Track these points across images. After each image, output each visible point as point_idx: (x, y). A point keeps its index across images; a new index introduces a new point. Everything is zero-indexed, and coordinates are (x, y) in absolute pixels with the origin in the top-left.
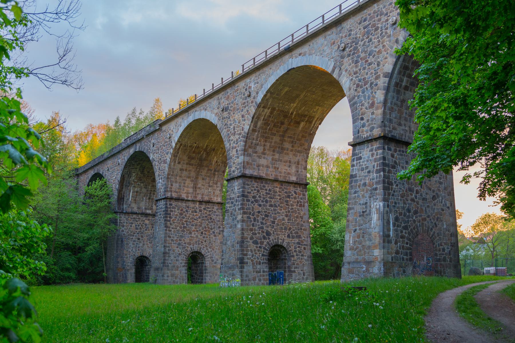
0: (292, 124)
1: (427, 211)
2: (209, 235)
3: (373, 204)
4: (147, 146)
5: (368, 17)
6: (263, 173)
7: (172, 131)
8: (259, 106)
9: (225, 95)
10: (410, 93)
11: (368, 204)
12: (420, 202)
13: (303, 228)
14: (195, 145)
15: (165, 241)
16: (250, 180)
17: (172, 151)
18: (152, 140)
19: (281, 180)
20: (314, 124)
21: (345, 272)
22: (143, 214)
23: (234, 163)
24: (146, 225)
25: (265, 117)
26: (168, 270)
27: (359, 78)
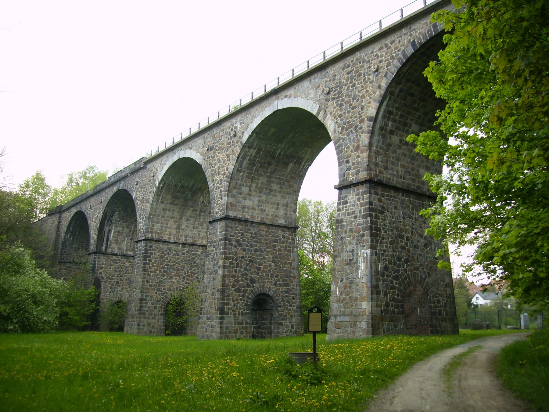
0: (280, 165)
1: (419, 259)
2: (192, 281)
3: (360, 251)
4: (130, 184)
5: (351, 64)
6: (249, 215)
7: (157, 169)
8: (244, 146)
9: (211, 134)
10: (395, 137)
11: (355, 251)
12: (412, 249)
13: (292, 275)
14: (180, 184)
15: (143, 286)
16: (234, 222)
17: (155, 190)
18: (136, 178)
19: (268, 223)
20: (304, 166)
21: (331, 326)
22: (123, 255)
23: (217, 204)
24: (126, 267)
25: (250, 157)
26: (145, 318)
27: (344, 121)
